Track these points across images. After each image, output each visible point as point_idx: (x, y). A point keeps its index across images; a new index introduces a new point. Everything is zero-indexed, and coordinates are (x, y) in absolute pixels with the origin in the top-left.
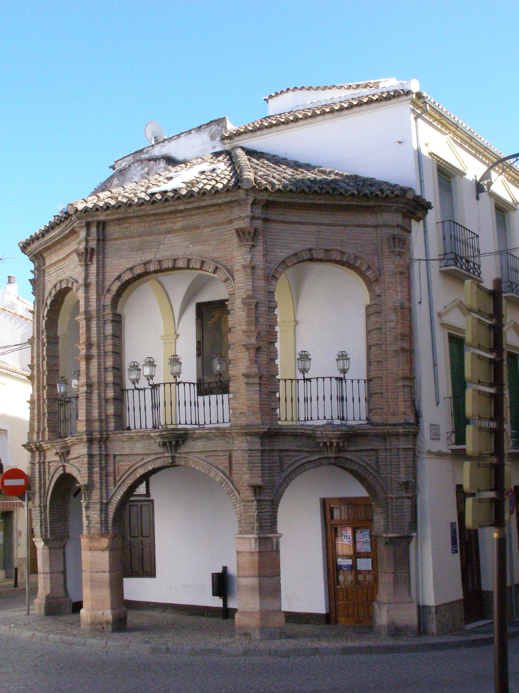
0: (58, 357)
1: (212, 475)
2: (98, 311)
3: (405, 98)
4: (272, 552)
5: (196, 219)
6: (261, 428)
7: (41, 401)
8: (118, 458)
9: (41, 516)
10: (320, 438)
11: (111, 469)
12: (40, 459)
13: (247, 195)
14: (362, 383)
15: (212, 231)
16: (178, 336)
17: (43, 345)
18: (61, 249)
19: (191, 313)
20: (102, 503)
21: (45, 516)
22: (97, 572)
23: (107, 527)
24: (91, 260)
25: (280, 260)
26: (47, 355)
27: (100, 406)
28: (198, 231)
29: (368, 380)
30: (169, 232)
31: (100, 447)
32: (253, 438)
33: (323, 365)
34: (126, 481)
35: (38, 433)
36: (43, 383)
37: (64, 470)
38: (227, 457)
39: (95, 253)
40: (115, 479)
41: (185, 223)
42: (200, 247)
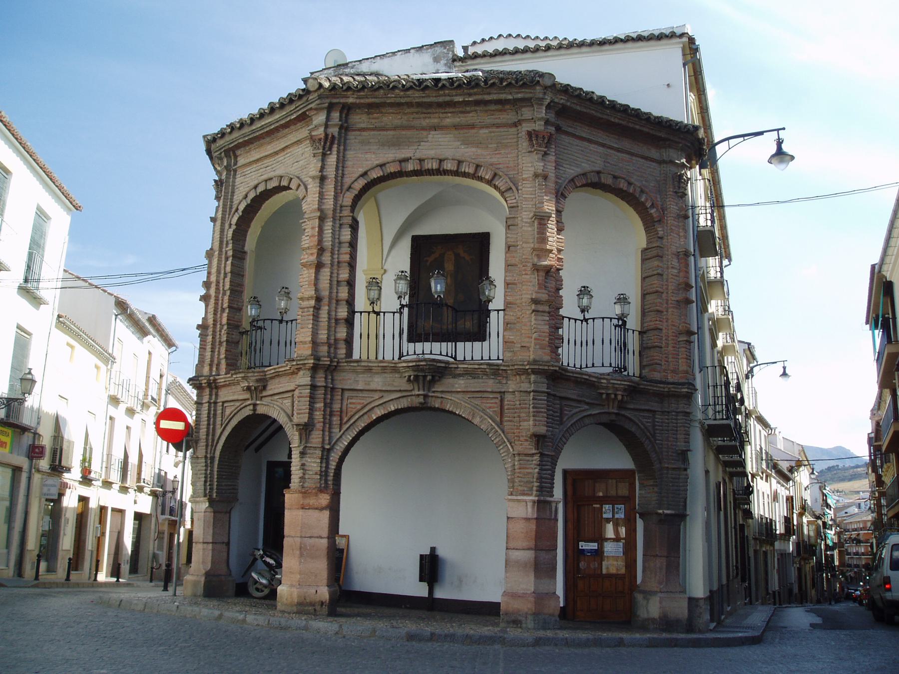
0: (243, 276)
1: (476, 421)
2: (334, 210)
3: (678, 40)
4: (550, 519)
5: (470, 118)
6: (553, 366)
7: (218, 326)
8: (347, 394)
9: (206, 470)
10: (603, 388)
11: (336, 406)
12: (210, 399)
13: (545, 93)
14: (636, 333)
15: (490, 132)
16: (385, 271)
17: (227, 259)
18: (270, 143)
19: (405, 247)
20: (323, 449)
21: (212, 471)
22: (310, 537)
23: (326, 481)
24: (330, 149)
25: (570, 178)
26: (231, 272)
27: (329, 327)
28: (473, 131)
29: (640, 333)
30: (435, 128)
31: (326, 378)
32: (539, 377)
33: (604, 305)
34: (357, 424)
35: (211, 365)
36: (222, 304)
37: (254, 410)
38: (498, 401)
39: (336, 142)
40: (341, 420)
41: (457, 120)
42: (474, 150)
